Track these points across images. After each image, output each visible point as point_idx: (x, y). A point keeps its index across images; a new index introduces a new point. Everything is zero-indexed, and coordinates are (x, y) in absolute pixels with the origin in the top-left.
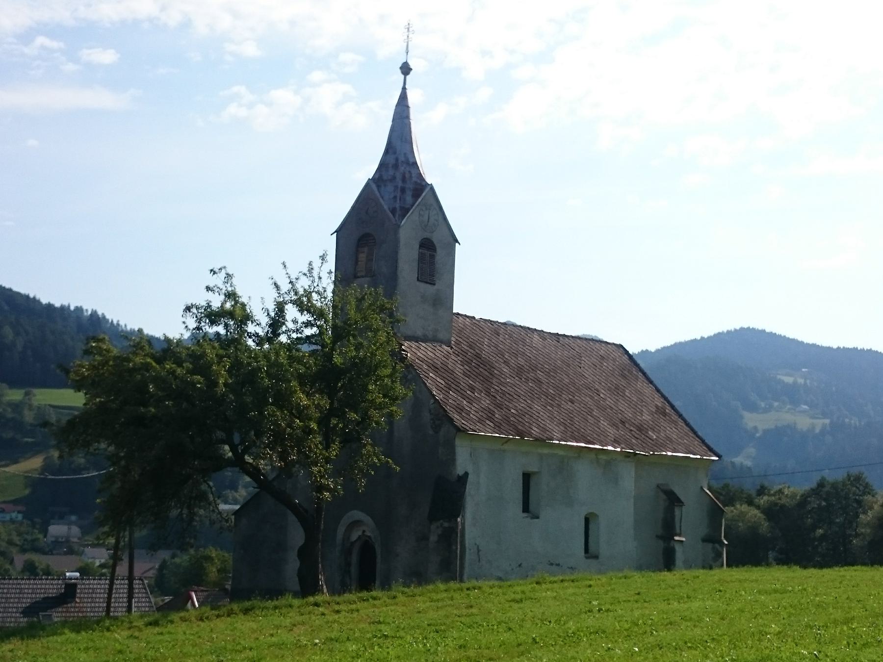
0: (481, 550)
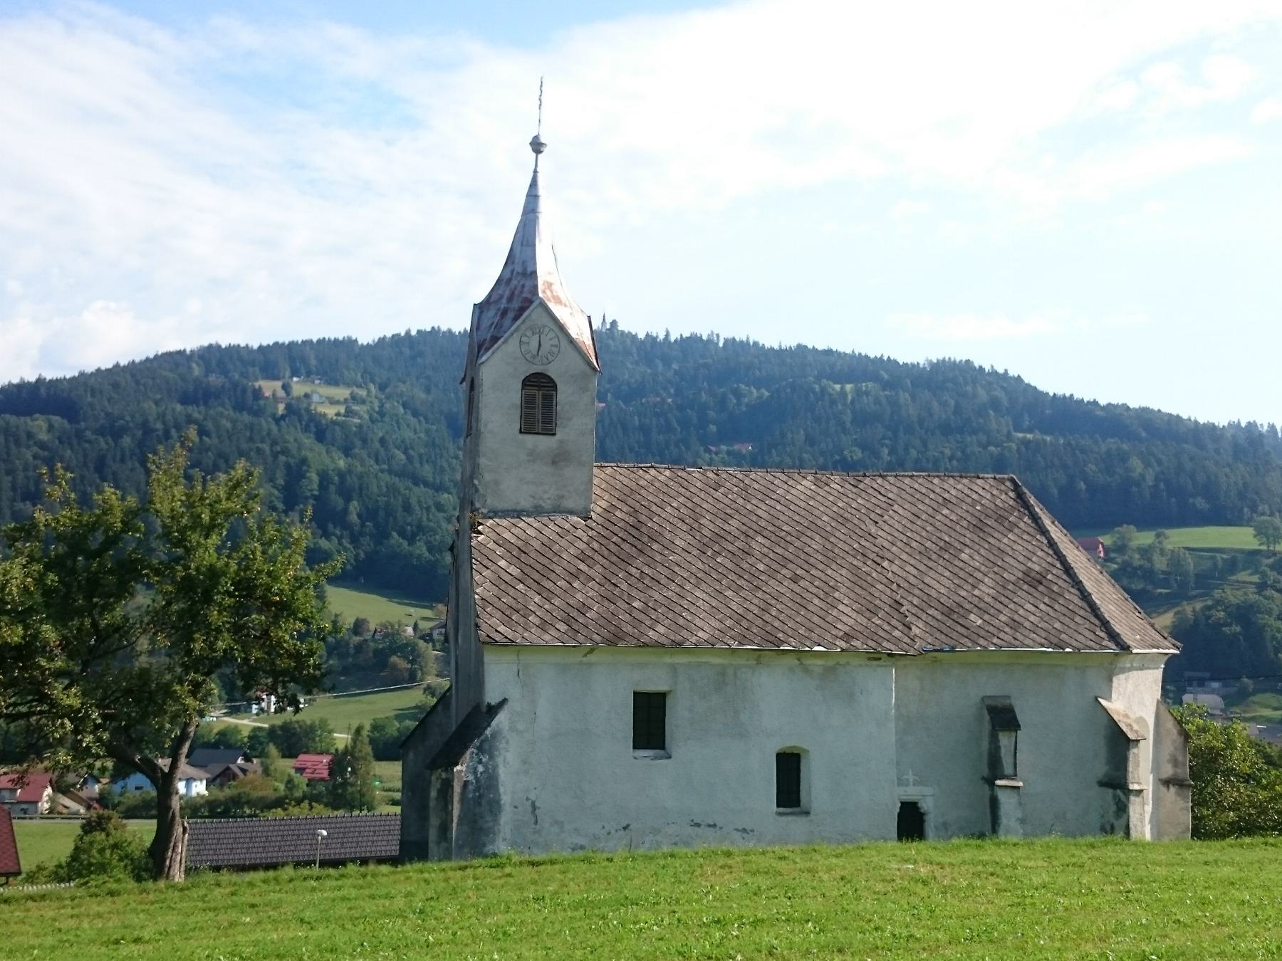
0: (539, 808)
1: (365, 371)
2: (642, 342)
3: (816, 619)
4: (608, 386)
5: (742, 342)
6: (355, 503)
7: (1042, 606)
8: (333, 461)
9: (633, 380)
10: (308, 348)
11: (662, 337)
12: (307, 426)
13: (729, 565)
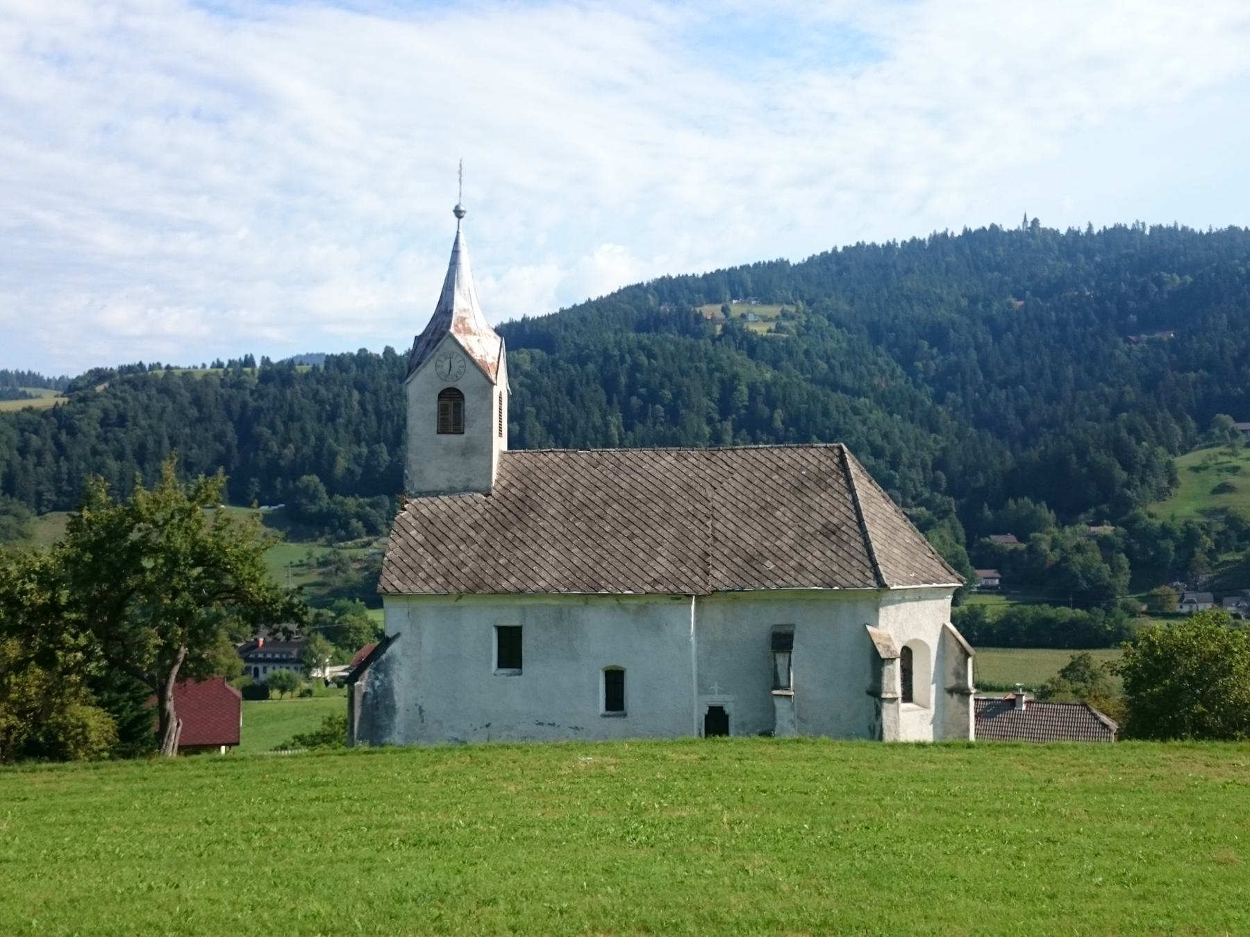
1: (796, 289)
2: (1064, 237)
3: (636, 569)
4: (1028, 284)
5: (1169, 229)
6: (779, 411)
7: (829, 553)
8: (761, 375)
9: (1053, 276)
10: (745, 273)
11: (1084, 230)
12: (741, 344)
13: (584, 527)
